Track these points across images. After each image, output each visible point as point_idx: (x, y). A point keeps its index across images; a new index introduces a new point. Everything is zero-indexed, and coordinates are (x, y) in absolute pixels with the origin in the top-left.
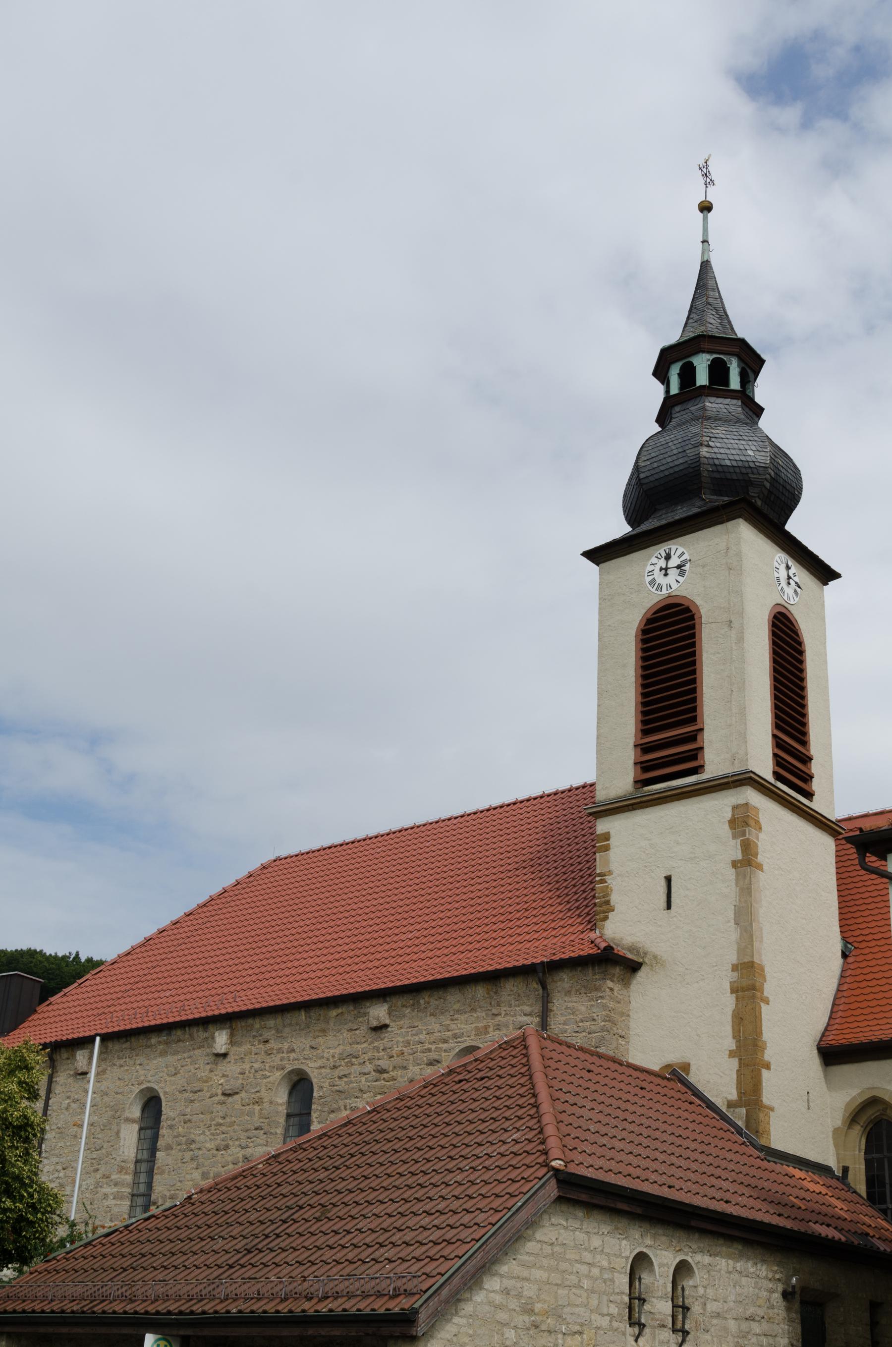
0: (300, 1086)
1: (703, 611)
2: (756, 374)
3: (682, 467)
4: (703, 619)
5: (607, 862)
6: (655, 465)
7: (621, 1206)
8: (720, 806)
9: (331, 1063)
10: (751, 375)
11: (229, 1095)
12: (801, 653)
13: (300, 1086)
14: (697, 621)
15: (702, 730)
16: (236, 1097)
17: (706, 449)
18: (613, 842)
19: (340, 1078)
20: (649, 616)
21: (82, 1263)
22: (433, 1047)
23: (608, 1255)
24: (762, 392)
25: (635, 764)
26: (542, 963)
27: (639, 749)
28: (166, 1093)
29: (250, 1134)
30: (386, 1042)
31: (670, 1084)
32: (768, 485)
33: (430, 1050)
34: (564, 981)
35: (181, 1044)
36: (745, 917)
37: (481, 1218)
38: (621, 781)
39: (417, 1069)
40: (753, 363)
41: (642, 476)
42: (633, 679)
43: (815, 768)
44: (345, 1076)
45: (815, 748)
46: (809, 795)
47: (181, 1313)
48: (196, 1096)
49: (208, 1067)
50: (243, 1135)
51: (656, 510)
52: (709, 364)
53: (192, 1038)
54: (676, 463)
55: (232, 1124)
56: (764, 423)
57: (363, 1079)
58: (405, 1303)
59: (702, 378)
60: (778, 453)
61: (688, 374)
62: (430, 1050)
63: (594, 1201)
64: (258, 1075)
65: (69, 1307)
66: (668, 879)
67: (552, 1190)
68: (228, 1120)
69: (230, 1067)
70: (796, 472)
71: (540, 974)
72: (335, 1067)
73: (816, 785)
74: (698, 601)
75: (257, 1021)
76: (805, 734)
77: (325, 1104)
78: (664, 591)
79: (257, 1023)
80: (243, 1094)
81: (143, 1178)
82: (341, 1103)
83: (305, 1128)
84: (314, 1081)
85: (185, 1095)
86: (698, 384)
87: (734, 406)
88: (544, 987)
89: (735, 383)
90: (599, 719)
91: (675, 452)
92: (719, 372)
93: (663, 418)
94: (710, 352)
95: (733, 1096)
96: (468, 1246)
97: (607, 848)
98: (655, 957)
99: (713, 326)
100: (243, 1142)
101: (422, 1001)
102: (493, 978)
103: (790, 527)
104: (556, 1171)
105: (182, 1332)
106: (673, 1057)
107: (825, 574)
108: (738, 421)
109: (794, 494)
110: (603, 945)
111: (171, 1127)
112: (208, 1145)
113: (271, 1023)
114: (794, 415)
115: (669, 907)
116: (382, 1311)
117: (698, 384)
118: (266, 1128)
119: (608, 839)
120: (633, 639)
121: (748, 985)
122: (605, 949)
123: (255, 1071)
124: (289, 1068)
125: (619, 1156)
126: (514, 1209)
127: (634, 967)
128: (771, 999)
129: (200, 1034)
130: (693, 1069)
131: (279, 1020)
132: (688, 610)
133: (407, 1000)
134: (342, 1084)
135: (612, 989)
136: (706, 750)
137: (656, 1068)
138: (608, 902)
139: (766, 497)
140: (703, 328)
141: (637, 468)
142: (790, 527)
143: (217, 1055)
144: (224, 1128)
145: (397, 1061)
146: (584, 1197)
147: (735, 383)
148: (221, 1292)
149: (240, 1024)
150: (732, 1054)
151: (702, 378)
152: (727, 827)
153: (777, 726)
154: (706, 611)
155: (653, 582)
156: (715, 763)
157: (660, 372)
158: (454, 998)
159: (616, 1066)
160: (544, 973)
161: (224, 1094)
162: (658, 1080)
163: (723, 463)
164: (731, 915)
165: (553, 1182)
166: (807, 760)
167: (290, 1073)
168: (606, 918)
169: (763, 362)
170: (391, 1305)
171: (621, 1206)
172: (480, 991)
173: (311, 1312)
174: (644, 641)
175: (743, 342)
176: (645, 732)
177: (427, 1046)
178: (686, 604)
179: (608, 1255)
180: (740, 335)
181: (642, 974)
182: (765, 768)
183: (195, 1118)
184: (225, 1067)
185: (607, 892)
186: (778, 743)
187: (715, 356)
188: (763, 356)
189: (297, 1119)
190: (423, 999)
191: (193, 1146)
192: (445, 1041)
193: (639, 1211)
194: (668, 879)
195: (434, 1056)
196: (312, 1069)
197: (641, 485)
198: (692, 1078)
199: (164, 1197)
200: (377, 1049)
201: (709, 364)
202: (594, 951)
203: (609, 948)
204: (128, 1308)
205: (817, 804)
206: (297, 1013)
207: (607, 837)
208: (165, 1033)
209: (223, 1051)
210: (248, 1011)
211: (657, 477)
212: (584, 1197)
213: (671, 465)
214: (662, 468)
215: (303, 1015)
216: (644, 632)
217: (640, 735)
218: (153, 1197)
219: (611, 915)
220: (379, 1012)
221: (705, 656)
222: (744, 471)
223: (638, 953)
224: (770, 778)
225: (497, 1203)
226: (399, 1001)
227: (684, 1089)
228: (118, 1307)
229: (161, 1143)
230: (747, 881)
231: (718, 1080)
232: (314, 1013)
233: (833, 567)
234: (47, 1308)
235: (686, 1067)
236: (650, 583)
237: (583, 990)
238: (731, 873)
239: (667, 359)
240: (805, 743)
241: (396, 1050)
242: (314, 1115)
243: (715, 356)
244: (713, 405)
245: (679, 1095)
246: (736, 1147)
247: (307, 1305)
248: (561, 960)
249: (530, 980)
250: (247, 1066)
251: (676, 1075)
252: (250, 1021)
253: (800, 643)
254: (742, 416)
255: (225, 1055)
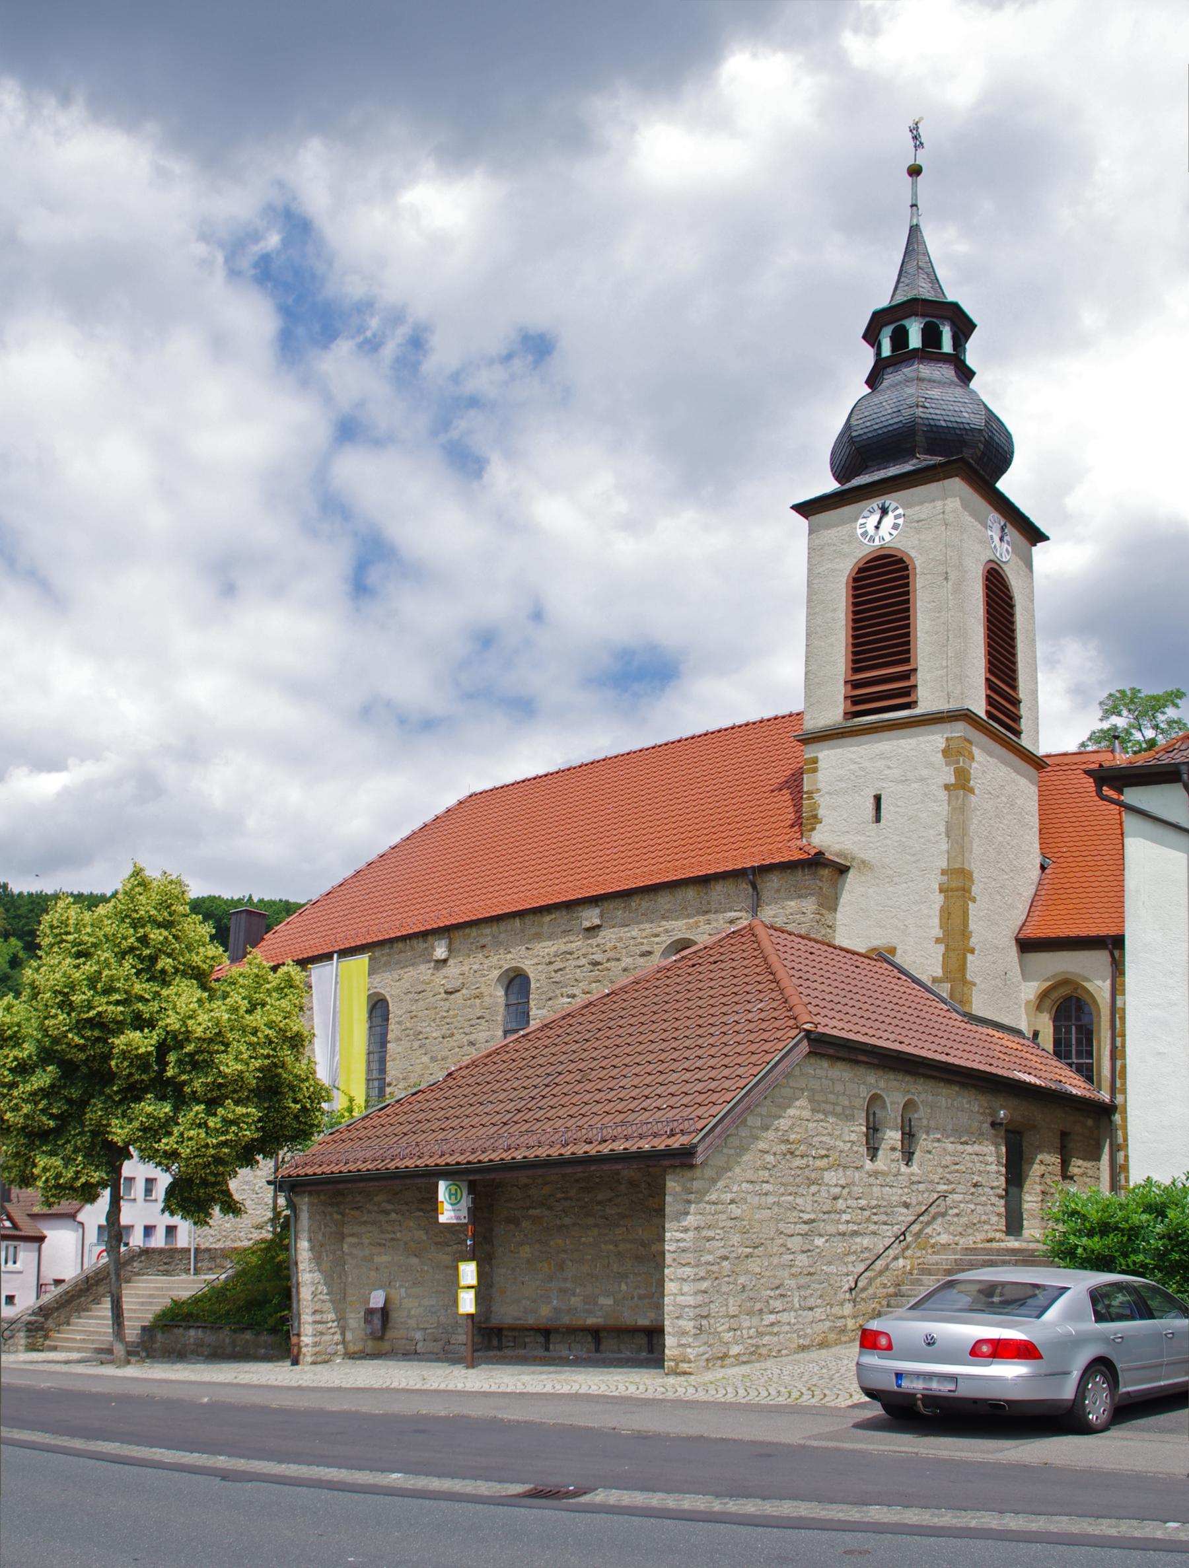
0: (517, 982)
1: (917, 563)
2: (967, 338)
3: (895, 427)
4: (918, 571)
5: (815, 782)
6: (868, 424)
7: (861, 1058)
8: (934, 741)
9: (547, 960)
10: (963, 339)
11: (451, 993)
12: (1012, 606)
13: (517, 982)
14: (910, 572)
15: (915, 670)
16: (458, 994)
17: (921, 409)
18: (820, 764)
19: (556, 971)
20: (860, 565)
21: (363, 1133)
22: (645, 941)
23: (849, 1096)
24: (972, 356)
25: (846, 698)
26: (753, 868)
27: (849, 686)
28: (391, 996)
29: (473, 1022)
30: (599, 940)
31: (879, 964)
32: (982, 447)
33: (642, 944)
34: (774, 882)
35: (403, 954)
36: (957, 831)
37: (740, 1071)
38: (833, 713)
39: (630, 960)
40: (964, 327)
41: (854, 434)
42: (844, 622)
43: (1024, 710)
44: (560, 970)
45: (1023, 693)
46: (1018, 733)
47: (469, 1163)
48: (420, 996)
49: (430, 971)
50: (466, 1024)
51: (867, 467)
52: (921, 328)
53: (412, 948)
54: (891, 422)
55: (455, 1016)
56: (973, 385)
57: (578, 971)
58: (684, 1140)
59: (915, 340)
60: (991, 417)
61: (900, 338)
62: (642, 944)
63: (840, 1055)
64: (477, 975)
65: (363, 1167)
66: (878, 799)
67: (805, 1047)
68: (451, 1012)
69: (452, 969)
70: (1008, 436)
71: (752, 878)
72: (551, 963)
73: (1024, 724)
74: (913, 554)
75: (474, 929)
76: (1015, 679)
77: (542, 994)
78: (877, 543)
79: (474, 932)
80: (464, 991)
81: (375, 1066)
82: (558, 992)
83: (525, 1017)
84: (531, 976)
85: (410, 996)
86: (911, 346)
87: (947, 372)
88: (754, 887)
89: (947, 346)
90: (807, 657)
91: (889, 411)
92: (931, 336)
93: (873, 381)
94: (923, 316)
95: (939, 973)
96: (734, 1093)
97: (815, 770)
98: (863, 862)
99: (925, 291)
100: (467, 1030)
101: (633, 904)
102: (704, 881)
103: (1001, 485)
104: (808, 1032)
105: (471, 1178)
106: (879, 940)
107: (1035, 536)
108: (952, 383)
109: (1005, 458)
110: (813, 852)
111: (399, 1023)
112: (434, 1035)
113: (487, 931)
114: (1011, 387)
115: (878, 819)
116: (662, 1147)
117: (911, 346)
118: (488, 1017)
119: (816, 763)
120: (844, 586)
121: (957, 888)
122: (816, 854)
123: (480, 971)
124: (506, 967)
125: (855, 1020)
126: (773, 1063)
127: (843, 870)
128: (978, 898)
129: (420, 945)
130: (899, 952)
131: (495, 928)
132: (901, 561)
133: (619, 903)
134: (558, 977)
135: (821, 888)
136: (919, 688)
137: (863, 951)
138: (815, 817)
139: (975, 456)
140: (915, 292)
141: (848, 426)
142: (1001, 485)
143: (437, 961)
144: (448, 1020)
145: (611, 954)
146: (831, 1051)
147: (947, 346)
148: (503, 1143)
149: (457, 935)
150: (938, 941)
151: (915, 340)
152: (940, 755)
153: (990, 671)
154: (920, 562)
155: (865, 534)
156: (928, 700)
157: (871, 336)
158: (664, 901)
159: (831, 950)
160: (754, 875)
161: (446, 992)
162: (867, 961)
163: (938, 423)
164: (943, 829)
165: (805, 1042)
166: (1016, 702)
167: (507, 971)
168: (814, 829)
169: (974, 326)
170: (670, 1141)
171: (861, 1058)
172: (690, 893)
173: (593, 1153)
174: (855, 588)
175: (955, 307)
176: (855, 670)
177: (639, 940)
178: (900, 555)
179: (849, 1096)
180: (951, 297)
181: (851, 875)
182: (980, 708)
183: (420, 1014)
184: (445, 971)
185: (814, 807)
186: (990, 684)
187: (928, 319)
188: (975, 321)
189: (514, 1007)
190: (634, 903)
191: (421, 1037)
192: (657, 936)
193: (876, 1061)
194: (878, 799)
195: (646, 948)
196: (528, 966)
197: (854, 442)
198: (898, 959)
199: (397, 1079)
200: (591, 946)
201: (921, 328)
202: (805, 856)
203: (820, 853)
204: (418, 1163)
205: (1025, 741)
206: (512, 921)
207: (815, 761)
208: (387, 946)
209: (443, 957)
210: (466, 922)
211: (870, 435)
212: (831, 1051)
213: (886, 424)
214: (876, 427)
215: (517, 922)
216: (855, 580)
217: (850, 672)
218: (388, 1080)
219: (818, 826)
220: (591, 916)
221: (919, 604)
222: (958, 432)
223: (846, 858)
224: (985, 718)
225: (754, 1059)
226: (609, 906)
227: (891, 968)
228: (409, 1163)
229: (390, 1036)
230: (960, 801)
231: (924, 958)
232: (528, 920)
233: (1043, 530)
234: (345, 1169)
235: (893, 951)
236: (862, 535)
237: (793, 889)
238: (943, 795)
239: (878, 320)
240: (1014, 688)
241: (609, 945)
242: (532, 1003)
243: (928, 319)
244: (926, 370)
245: (887, 973)
246: (943, 1013)
247: (587, 1148)
248: (771, 864)
249: (740, 881)
250: (466, 968)
251: (883, 956)
252: (467, 931)
253: (1011, 598)
254: (955, 379)
255: (445, 961)
